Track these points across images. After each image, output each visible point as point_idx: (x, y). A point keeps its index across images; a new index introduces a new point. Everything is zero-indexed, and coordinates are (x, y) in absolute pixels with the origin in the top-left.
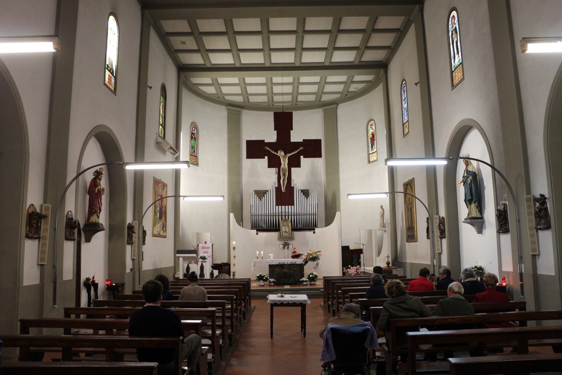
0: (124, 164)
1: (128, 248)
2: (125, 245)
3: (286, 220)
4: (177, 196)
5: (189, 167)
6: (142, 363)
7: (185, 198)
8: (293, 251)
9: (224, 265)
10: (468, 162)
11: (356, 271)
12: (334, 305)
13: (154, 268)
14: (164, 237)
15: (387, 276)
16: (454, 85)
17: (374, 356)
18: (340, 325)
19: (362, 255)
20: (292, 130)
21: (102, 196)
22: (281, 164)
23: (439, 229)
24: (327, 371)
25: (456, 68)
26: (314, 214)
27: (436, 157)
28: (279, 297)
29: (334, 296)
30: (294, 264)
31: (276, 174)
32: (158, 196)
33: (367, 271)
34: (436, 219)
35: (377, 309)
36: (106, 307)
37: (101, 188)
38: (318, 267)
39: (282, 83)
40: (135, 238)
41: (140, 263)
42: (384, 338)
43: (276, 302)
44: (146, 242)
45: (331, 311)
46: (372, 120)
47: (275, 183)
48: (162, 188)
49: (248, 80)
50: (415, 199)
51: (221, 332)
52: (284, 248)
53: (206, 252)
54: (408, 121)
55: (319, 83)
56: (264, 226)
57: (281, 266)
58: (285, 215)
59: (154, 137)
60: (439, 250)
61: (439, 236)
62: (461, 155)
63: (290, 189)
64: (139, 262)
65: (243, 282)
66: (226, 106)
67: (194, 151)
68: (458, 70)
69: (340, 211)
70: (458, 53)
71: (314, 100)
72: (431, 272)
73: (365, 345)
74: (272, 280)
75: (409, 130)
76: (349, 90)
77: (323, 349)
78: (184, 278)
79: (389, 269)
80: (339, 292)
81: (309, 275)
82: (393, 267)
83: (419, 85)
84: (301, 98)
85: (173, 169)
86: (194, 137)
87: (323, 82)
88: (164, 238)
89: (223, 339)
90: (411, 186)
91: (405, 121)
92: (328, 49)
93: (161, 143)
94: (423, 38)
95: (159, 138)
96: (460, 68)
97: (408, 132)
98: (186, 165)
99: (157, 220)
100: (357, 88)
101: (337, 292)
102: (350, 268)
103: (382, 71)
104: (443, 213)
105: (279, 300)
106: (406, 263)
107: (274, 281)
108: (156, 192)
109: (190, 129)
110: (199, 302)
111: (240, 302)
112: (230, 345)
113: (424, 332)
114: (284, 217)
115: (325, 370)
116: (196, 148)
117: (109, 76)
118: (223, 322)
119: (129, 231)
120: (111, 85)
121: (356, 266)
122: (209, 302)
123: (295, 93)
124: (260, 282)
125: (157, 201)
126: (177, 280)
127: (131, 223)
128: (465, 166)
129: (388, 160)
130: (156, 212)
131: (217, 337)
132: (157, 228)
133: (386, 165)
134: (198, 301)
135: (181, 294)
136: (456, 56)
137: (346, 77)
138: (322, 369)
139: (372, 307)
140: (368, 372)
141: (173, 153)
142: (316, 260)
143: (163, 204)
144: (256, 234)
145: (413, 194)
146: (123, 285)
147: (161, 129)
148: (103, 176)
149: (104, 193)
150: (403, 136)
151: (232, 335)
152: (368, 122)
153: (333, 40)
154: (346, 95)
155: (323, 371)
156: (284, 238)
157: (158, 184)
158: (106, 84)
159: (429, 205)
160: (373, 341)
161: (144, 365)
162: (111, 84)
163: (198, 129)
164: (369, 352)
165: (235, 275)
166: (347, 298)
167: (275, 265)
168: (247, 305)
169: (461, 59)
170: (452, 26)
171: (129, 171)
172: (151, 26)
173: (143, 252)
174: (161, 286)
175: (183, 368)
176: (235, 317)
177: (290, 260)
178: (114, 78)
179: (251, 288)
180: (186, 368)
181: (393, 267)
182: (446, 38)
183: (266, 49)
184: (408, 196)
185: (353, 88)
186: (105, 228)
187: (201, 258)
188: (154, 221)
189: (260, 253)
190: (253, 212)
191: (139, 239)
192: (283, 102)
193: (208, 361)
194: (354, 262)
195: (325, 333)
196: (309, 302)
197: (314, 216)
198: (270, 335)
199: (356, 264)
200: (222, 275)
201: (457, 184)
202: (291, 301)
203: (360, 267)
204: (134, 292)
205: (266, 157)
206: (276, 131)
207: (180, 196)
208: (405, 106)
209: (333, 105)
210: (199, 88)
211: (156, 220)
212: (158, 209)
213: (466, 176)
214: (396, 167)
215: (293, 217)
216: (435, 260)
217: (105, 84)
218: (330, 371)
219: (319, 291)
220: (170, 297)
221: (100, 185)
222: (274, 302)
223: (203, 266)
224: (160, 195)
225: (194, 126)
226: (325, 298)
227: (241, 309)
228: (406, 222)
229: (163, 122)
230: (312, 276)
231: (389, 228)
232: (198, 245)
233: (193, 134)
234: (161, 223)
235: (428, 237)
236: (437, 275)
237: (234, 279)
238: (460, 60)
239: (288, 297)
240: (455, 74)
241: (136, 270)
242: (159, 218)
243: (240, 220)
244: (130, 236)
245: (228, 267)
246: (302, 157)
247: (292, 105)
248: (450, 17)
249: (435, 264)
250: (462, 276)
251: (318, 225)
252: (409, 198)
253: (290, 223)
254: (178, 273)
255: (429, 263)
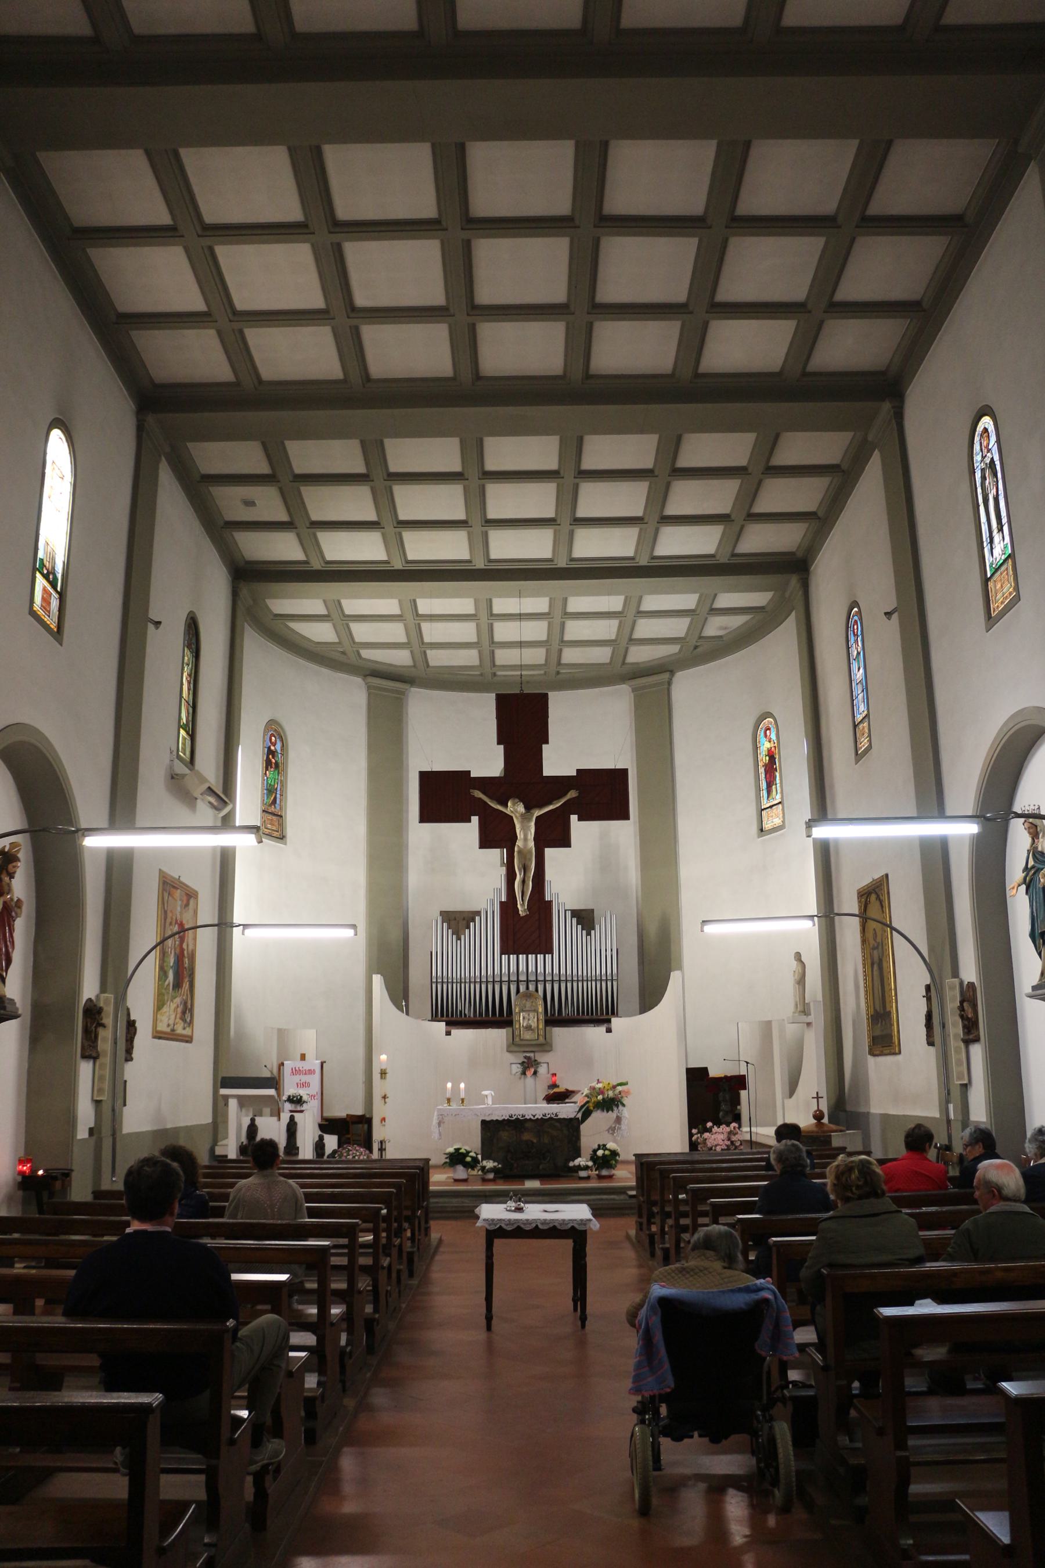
0: (80, 833)
1: (85, 1069)
2: (76, 1061)
3: (528, 995)
4: (226, 924)
5: (260, 842)
6: (115, 1394)
7: (248, 931)
8: (551, 1083)
9: (354, 1123)
10: (1036, 826)
11: (729, 1139)
12: (667, 1236)
13: (155, 1128)
14: (187, 1039)
15: (816, 1150)
16: (993, 615)
17: (783, 1383)
18: (684, 1288)
19: (743, 1094)
20: (547, 742)
21: (14, 921)
22: (515, 838)
23: (962, 1017)
24: (649, 1425)
25: (997, 570)
26: (609, 978)
27: (948, 813)
28: (510, 1211)
29: (668, 1209)
30: (551, 1118)
31: (501, 866)
32: (171, 924)
33: (761, 1140)
34: (952, 988)
35: (789, 1245)
36: (16, 1236)
37: (11, 899)
38: (619, 1128)
39: (520, 615)
40: (105, 1040)
41: (117, 1111)
42: (812, 1328)
43: (503, 1225)
44: (135, 1054)
45: (659, 1253)
46: (769, 715)
47: (500, 890)
48: (185, 902)
49: (425, 606)
50: (891, 933)
51: (345, 1310)
52: (524, 1073)
53: (305, 1085)
54: (867, 716)
55: (619, 613)
56: (467, 1012)
57: (516, 1124)
58: (528, 981)
59: (166, 758)
60: (964, 1076)
61: (962, 1036)
62: (1017, 808)
63: (541, 906)
64: (113, 1110)
65: (408, 1168)
66: (365, 676)
67: (274, 802)
68: (1001, 574)
69: (680, 968)
70: (1001, 529)
71: (608, 661)
72: (940, 1139)
73: (756, 1347)
74: (489, 1164)
75: (870, 741)
76: (704, 634)
77: (638, 1359)
78: (241, 1158)
79: (824, 1132)
80: (680, 1197)
81: (595, 1151)
82: (833, 1127)
83: (895, 616)
84: (570, 656)
85: (214, 848)
86: (273, 761)
87: (632, 611)
88: (187, 1042)
89: (350, 1332)
90: (878, 898)
91: (859, 718)
92: (646, 521)
93: (183, 776)
94: (902, 461)
95: (177, 762)
96: (1007, 569)
97: (870, 747)
98: (253, 836)
99: (168, 993)
100: (726, 628)
101: (676, 1197)
102: (711, 1131)
103: (794, 581)
104: (969, 972)
105: (509, 1220)
106: (868, 1113)
107: (495, 1167)
108: (166, 912)
109: (264, 741)
110: (281, 1225)
111: (400, 1227)
112: (370, 1349)
113: (926, 1307)
114: (525, 986)
115: (642, 1422)
116: (278, 792)
117: (45, 589)
118: (351, 1282)
119: (87, 1023)
120: (49, 617)
121: (728, 1125)
122: (312, 1224)
123: (556, 643)
124: (455, 1171)
125: (169, 937)
126: (220, 1162)
127: (93, 998)
128: (1030, 840)
129: (816, 823)
130: (166, 968)
131: (332, 1324)
132: (168, 1013)
133: (809, 836)
134: (279, 1222)
135: (232, 1201)
136: (997, 538)
137: (696, 597)
138: (635, 1417)
139: (774, 1239)
140: (766, 1426)
141: (215, 804)
142: (615, 1108)
143: (185, 946)
144: (446, 1035)
145: (884, 921)
146: (67, 1175)
147: (184, 739)
148: (19, 864)
149: (21, 914)
150: (856, 759)
151: (374, 1320)
152: (757, 721)
153: (659, 497)
154: (696, 647)
155: (635, 1425)
156: (524, 1045)
157: (174, 890)
158: (35, 611)
159: (931, 949)
160: (778, 1337)
161: (123, 1401)
162: (49, 612)
163: (286, 739)
164: (769, 1368)
165: (385, 1150)
166: (704, 1214)
167: (497, 1120)
168: (419, 1235)
169: (1009, 545)
170: (983, 457)
171: (94, 850)
172: (163, 459)
173: (126, 1081)
174: (178, 1174)
175: (232, 1412)
176: (383, 1268)
177: (541, 1109)
178: (57, 596)
179: (431, 1188)
180: (244, 1414)
181: (831, 1125)
182: (965, 487)
183: (473, 474)
184: (872, 925)
185: (715, 627)
186: (20, 1012)
187: (290, 1100)
188: (158, 996)
189: (456, 1088)
190: (438, 971)
191: (116, 1043)
192: (521, 667)
193: (306, 1394)
194: (721, 1114)
195: (643, 1312)
196: (595, 1225)
197: (609, 984)
198: (484, 1322)
199: (729, 1118)
200: (349, 1150)
201: (1007, 889)
202: (544, 1222)
203: (740, 1127)
204: (98, 1194)
205: (475, 819)
206: (502, 747)
207: (232, 926)
208: (859, 675)
209: (662, 675)
210: (293, 630)
211: (164, 991)
212: (171, 960)
213: (1033, 867)
214: (837, 841)
215: (549, 987)
216: (951, 1106)
217: (33, 613)
218: (657, 1424)
219: (622, 1197)
220: (202, 1209)
221: (10, 891)
222: (495, 1225)
223: (296, 1124)
224: (176, 922)
225: (275, 732)
226: (640, 1216)
227: (400, 1246)
228: (867, 999)
229: (190, 718)
230: (603, 1154)
231: (818, 1016)
232: (283, 1064)
233: (271, 753)
234: (178, 1000)
235: (931, 1039)
236: (958, 1148)
237: (381, 1160)
238: (1005, 547)
239: (535, 1212)
240: (995, 587)
241: (106, 1131)
242: (173, 986)
243: (400, 996)
244: (90, 1036)
245: (366, 1126)
246: (574, 818)
247: (545, 673)
248: (977, 433)
249: (952, 1116)
250: (1030, 1148)
251: (621, 1008)
252: (874, 929)
253: (541, 1002)
254: (224, 1142)
255: (934, 1113)
